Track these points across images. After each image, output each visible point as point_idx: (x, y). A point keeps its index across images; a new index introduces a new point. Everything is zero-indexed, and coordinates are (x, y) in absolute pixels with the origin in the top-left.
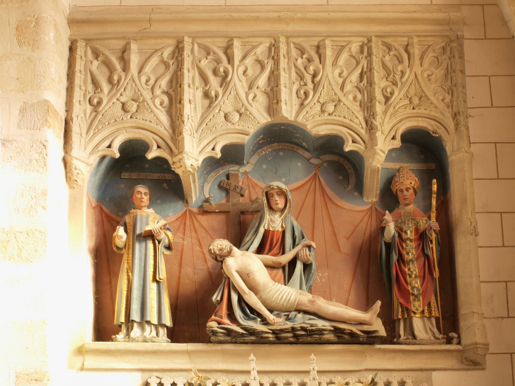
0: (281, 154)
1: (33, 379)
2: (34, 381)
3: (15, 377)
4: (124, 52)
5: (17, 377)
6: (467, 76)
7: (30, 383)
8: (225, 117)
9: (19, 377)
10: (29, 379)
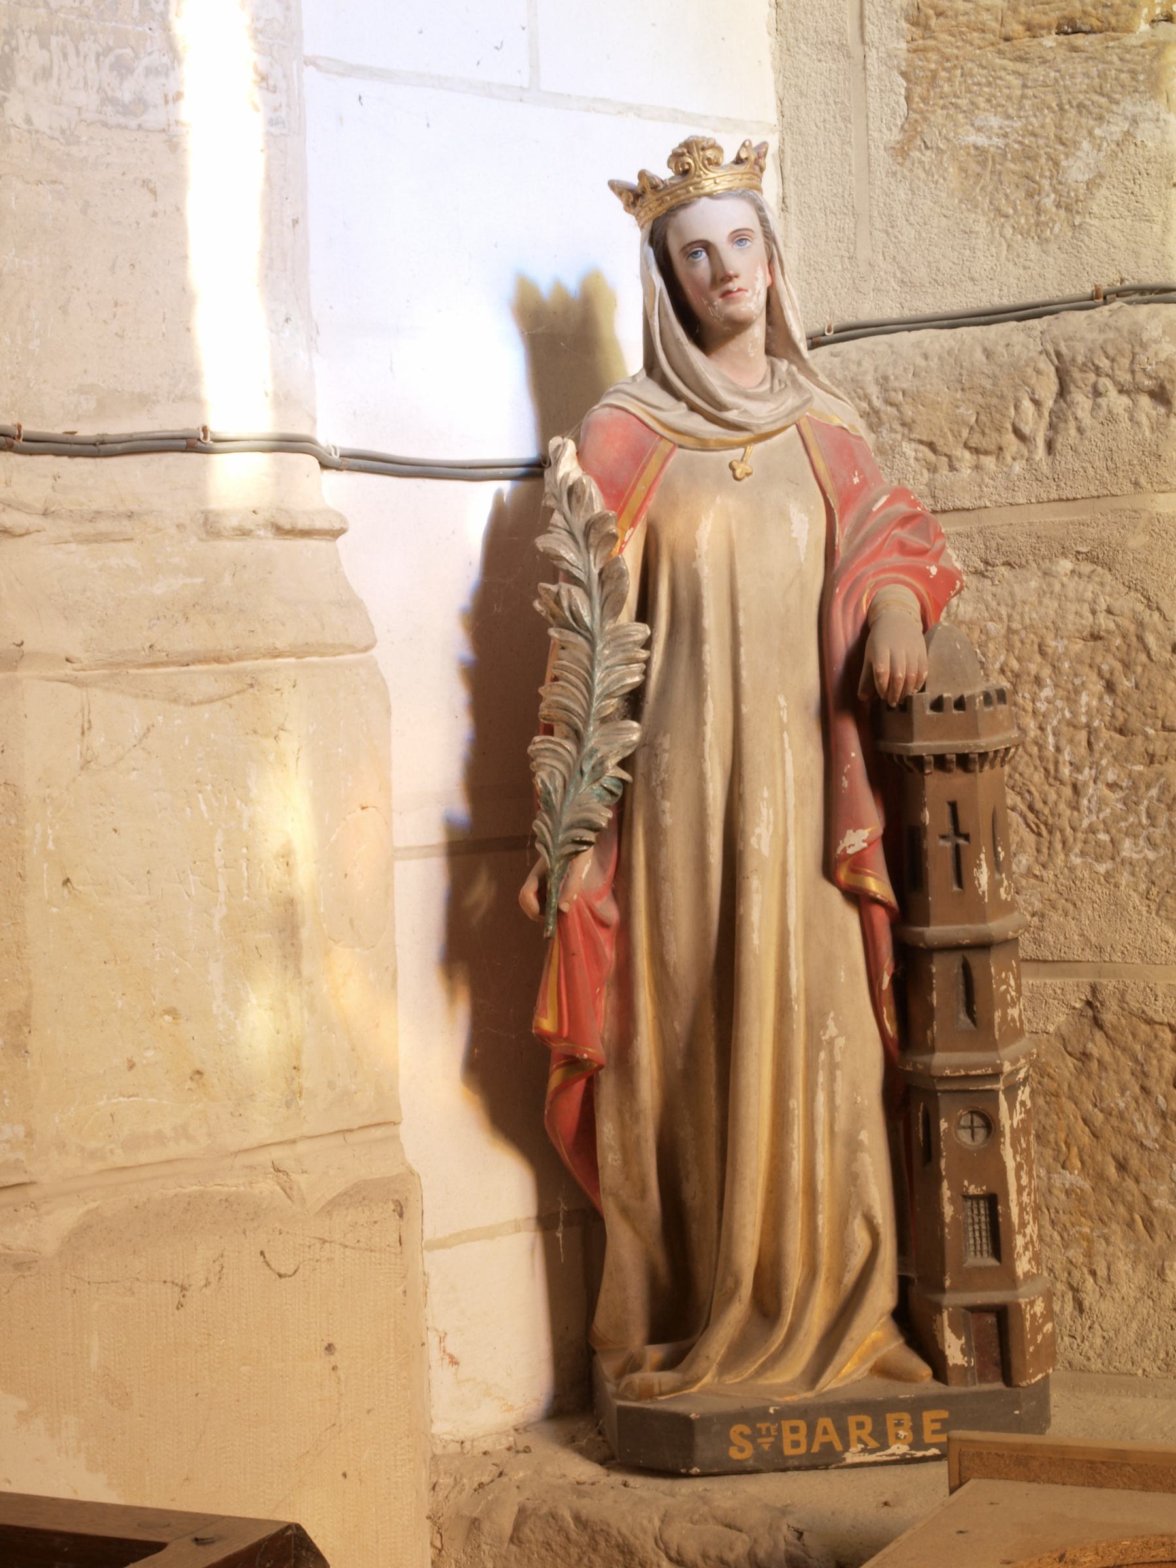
0: (948, 1072)
1: (1044, 20)
2: (1050, 41)
3: (904, 25)
4: (1149, 840)
5: (915, 24)
6: (310, 62)
7: (1021, 59)
8: (835, 356)
9: (933, 22)
10: (1017, 28)
